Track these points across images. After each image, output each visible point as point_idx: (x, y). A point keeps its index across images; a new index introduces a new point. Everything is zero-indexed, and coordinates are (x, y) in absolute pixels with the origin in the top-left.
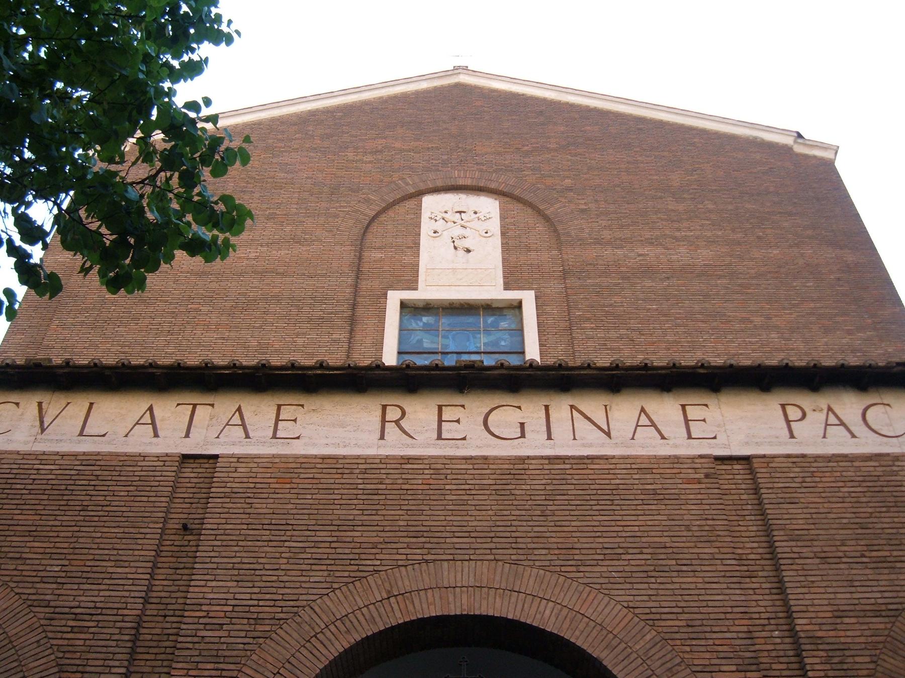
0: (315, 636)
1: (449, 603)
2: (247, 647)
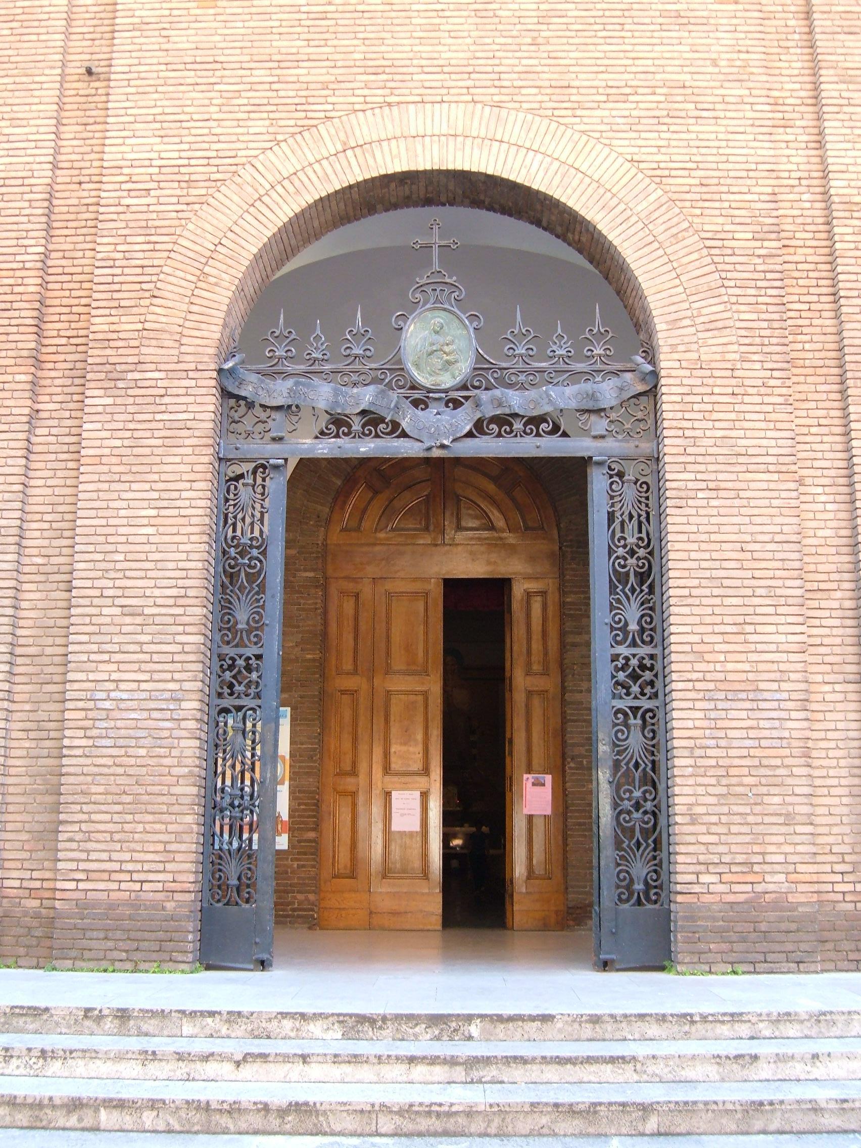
0: (260, 199)
1: (416, 156)
2: (180, 215)
